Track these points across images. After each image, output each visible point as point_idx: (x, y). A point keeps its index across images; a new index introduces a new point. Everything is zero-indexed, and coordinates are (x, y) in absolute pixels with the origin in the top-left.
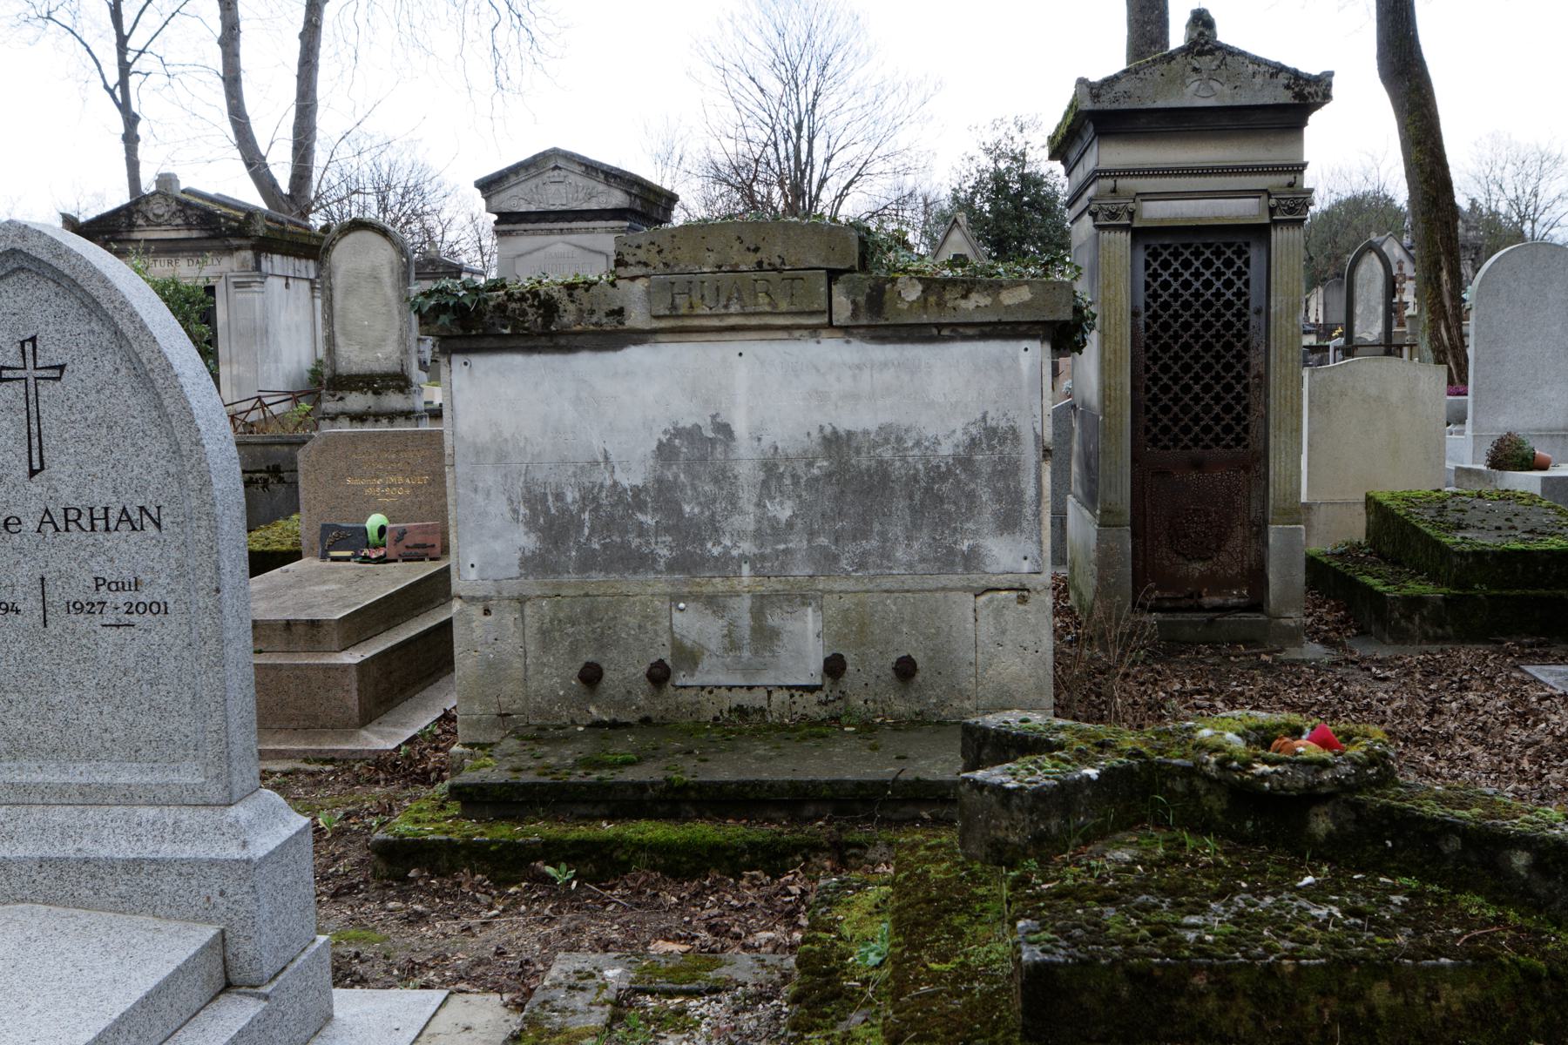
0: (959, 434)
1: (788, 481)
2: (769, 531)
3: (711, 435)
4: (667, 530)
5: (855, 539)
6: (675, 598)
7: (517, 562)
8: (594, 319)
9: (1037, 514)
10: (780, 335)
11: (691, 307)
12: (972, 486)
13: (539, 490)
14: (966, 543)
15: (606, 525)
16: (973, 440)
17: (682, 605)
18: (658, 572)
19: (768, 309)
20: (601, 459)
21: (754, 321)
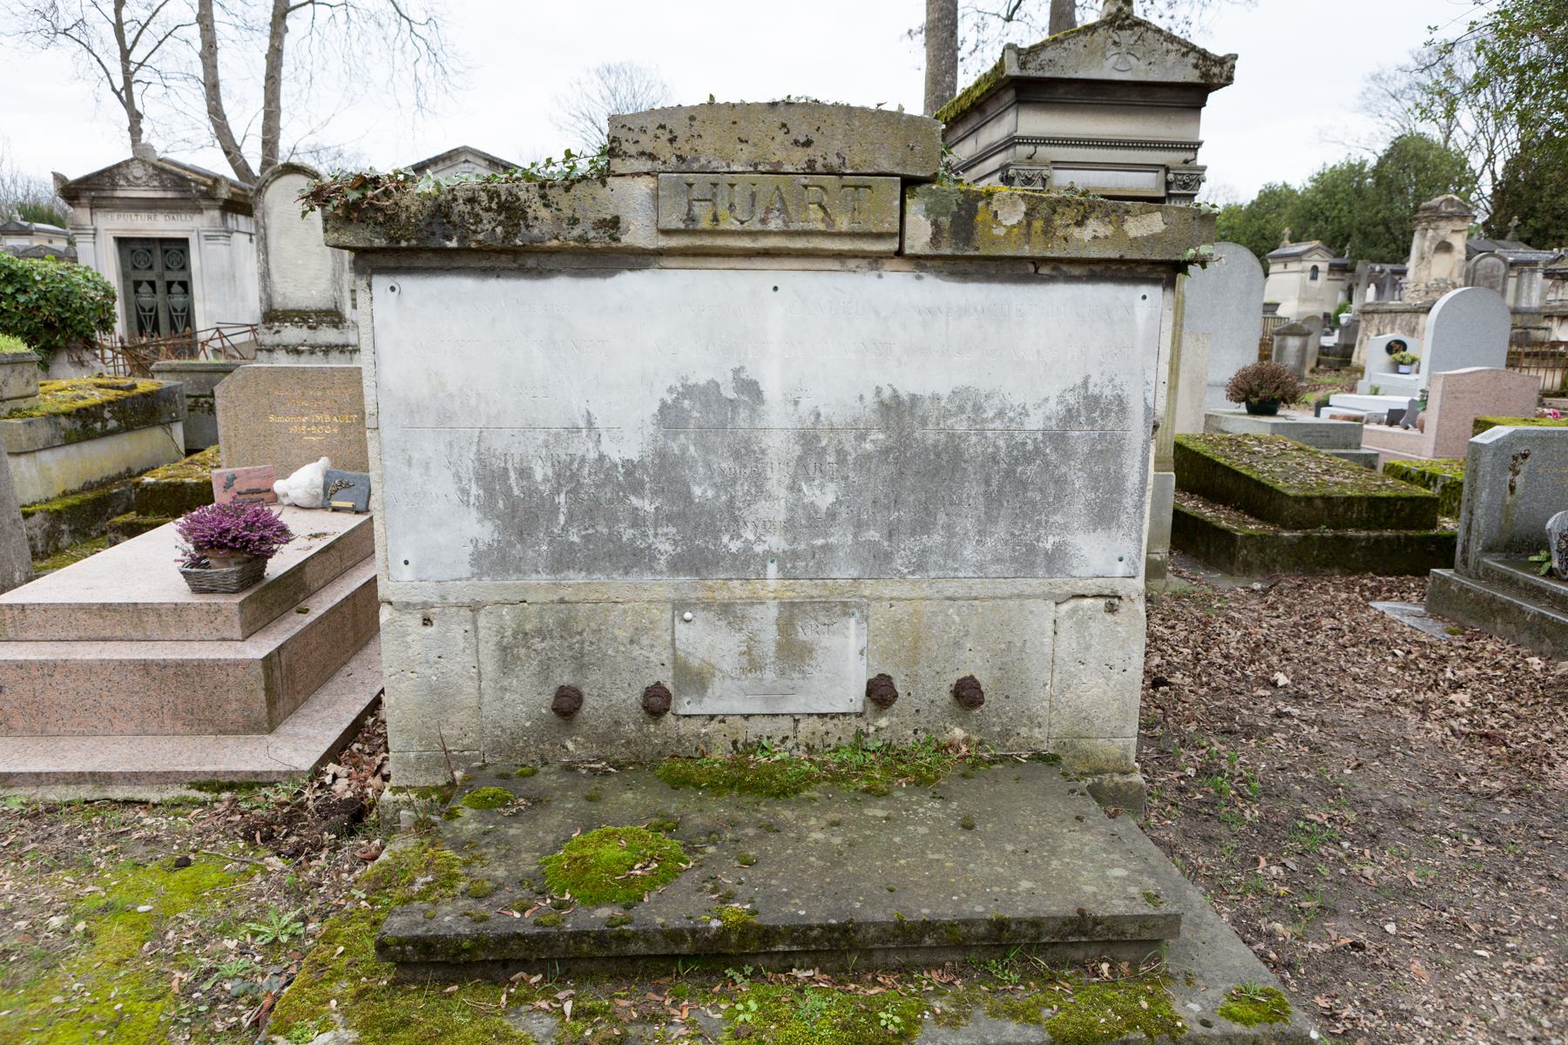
0: (1052, 404)
1: (831, 459)
2: (804, 521)
3: (732, 395)
4: (670, 519)
5: (913, 533)
6: (679, 606)
7: (468, 559)
8: (577, 232)
9: (1139, 506)
10: (830, 264)
12: (1064, 469)
13: (498, 464)
14: (1051, 539)
15: (588, 512)
16: (1069, 411)
17: (688, 615)
18: (655, 572)
19: (821, 227)
20: (582, 424)
21: (799, 244)
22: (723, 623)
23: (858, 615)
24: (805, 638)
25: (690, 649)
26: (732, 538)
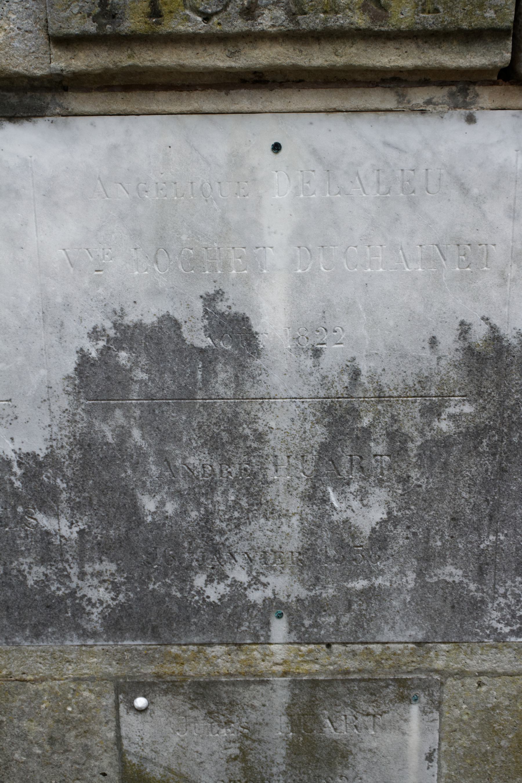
1: (379, 447)
2: (333, 551)
3: (203, 341)
4: (105, 549)
6: (126, 688)
10: (376, 98)
11: (155, 13)
17: (141, 702)
18: (85, 634)
19: (361, 20)
21: (319, 57)
22: (199, 714)
23: (423, 699)
24: (335, 735)
25: (147, 752)
26: (210, 580)
